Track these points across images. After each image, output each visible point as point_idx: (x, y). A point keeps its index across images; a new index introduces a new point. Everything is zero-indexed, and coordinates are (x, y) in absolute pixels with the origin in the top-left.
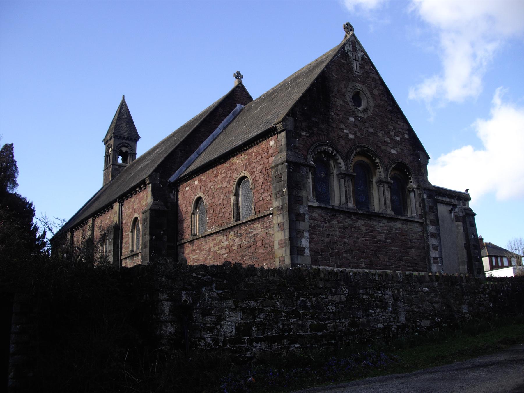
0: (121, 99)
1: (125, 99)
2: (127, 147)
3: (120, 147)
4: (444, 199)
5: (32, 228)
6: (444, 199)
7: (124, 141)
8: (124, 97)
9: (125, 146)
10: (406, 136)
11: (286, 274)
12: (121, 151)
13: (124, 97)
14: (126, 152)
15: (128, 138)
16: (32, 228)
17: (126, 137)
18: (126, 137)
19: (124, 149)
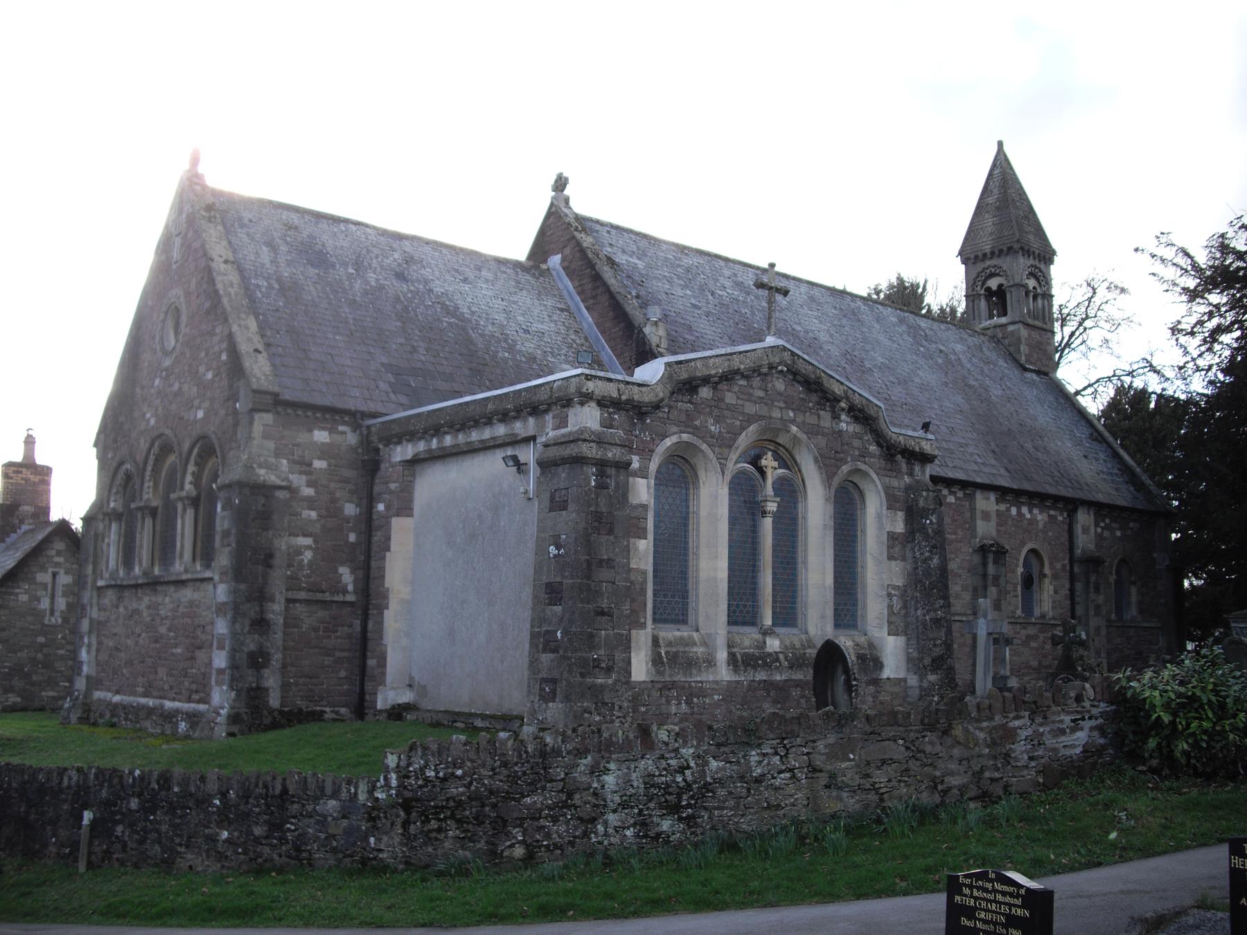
0: (547, 196)
1: (1006, 148)
2: (998, 275)
3: (984, 283)
4: (487, 433)
5: (1152, 405)
6: (487, 433)
7: (988, 263)
8: (1000, 144)
9: (992, 275)
10: (1190, 646)
11: (224, 795)
12: (988, 289)
13: (1000, 144)
14: (1000, 286)
15: (992, 253)
16: (1152, 405)
17: (988, 251)
18: (988, 251)
19: (993, 284)
